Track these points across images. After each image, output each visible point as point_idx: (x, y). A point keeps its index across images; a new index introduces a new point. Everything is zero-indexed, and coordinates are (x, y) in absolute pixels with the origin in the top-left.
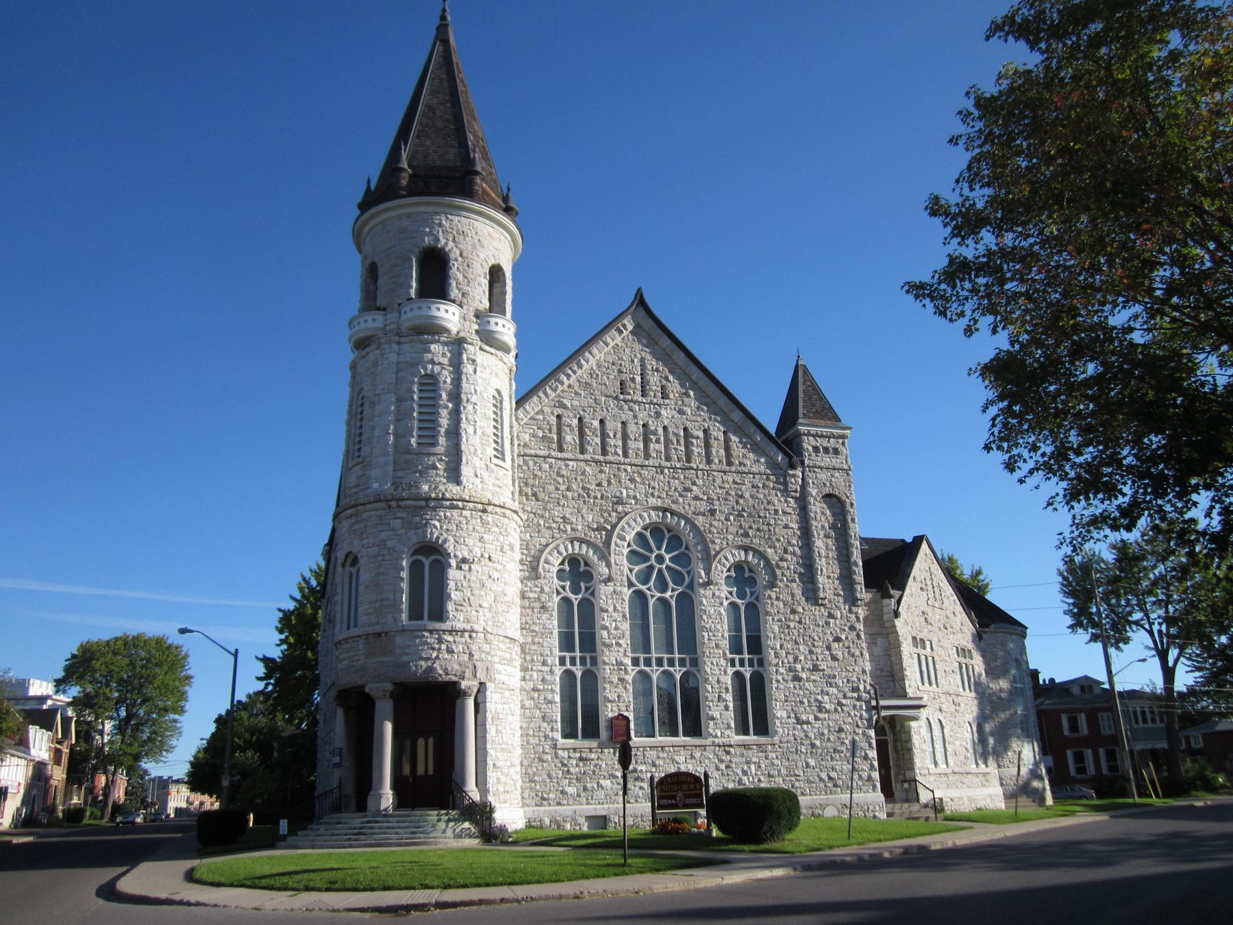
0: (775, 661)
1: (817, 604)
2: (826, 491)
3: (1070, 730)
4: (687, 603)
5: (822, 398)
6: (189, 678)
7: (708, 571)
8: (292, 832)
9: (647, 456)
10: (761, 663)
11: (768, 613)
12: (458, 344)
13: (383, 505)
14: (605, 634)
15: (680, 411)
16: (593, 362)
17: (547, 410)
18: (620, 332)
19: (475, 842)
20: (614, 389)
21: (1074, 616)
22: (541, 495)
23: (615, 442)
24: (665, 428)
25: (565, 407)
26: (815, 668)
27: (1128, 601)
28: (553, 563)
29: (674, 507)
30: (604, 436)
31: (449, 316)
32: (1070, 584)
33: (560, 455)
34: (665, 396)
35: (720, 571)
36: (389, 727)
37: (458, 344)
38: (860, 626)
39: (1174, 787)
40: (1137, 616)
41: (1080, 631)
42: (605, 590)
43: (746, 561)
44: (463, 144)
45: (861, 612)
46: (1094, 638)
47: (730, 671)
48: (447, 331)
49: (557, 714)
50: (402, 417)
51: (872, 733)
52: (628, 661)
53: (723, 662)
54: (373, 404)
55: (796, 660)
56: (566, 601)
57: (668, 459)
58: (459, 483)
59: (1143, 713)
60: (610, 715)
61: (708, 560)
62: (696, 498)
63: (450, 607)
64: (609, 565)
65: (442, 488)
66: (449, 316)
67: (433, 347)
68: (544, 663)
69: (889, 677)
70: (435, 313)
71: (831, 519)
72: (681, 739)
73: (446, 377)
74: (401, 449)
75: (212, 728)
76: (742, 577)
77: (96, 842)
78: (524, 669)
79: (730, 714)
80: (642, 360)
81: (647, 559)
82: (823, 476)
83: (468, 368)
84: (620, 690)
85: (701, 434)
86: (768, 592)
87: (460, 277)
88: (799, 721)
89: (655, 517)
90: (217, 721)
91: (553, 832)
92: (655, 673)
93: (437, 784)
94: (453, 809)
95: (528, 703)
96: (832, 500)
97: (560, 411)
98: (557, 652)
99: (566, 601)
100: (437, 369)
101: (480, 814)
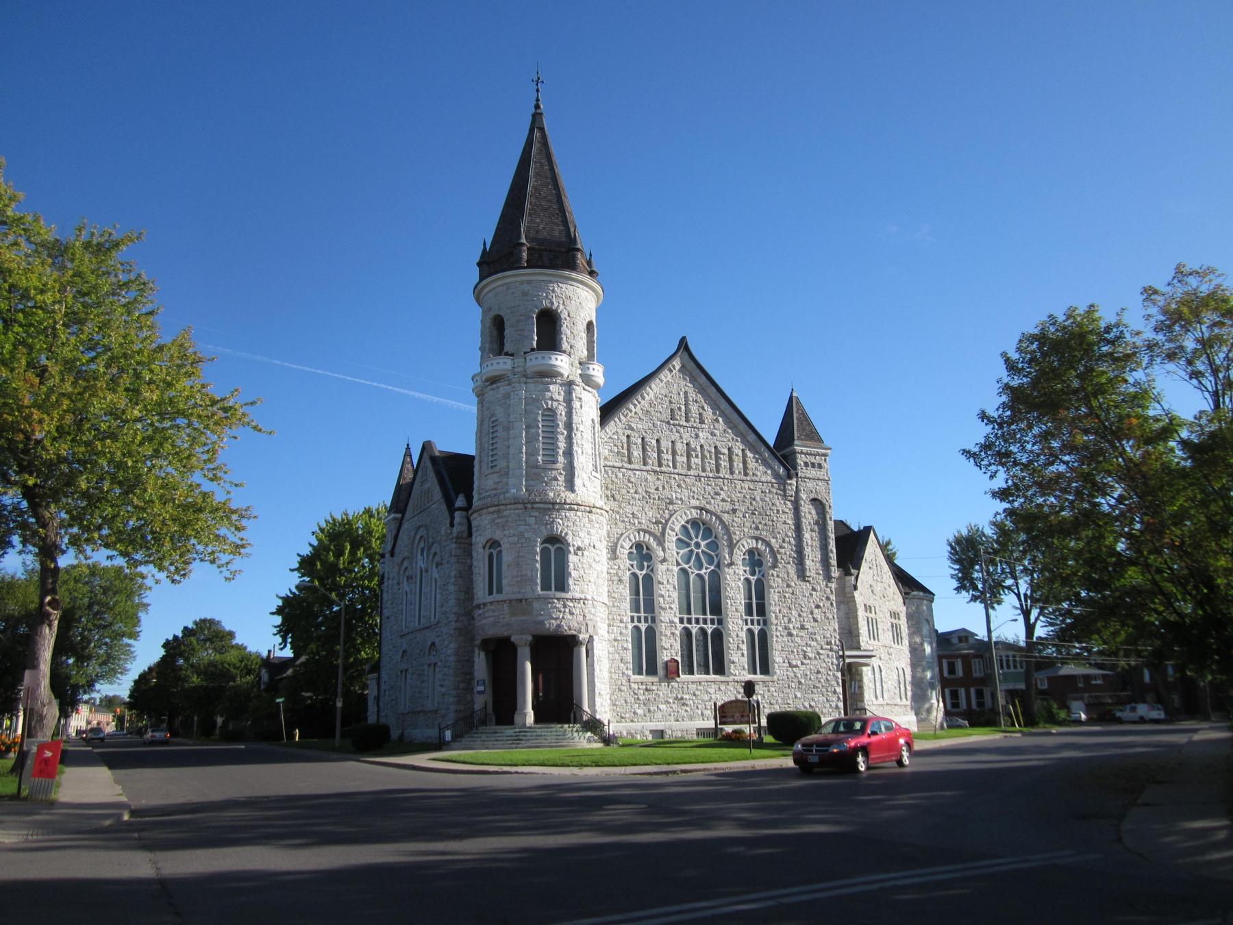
0: (775, 622)
1: (804, 580)
2: (813, 496)
3: (960, 672)
4: (716, 579)
5: (810, 424)
6: (146, 605)
7: (731, 554)
8: (456, 737)
9: (689, 468)
10: (765, 623)
11: (771, 587)
12: (569, 385)
13: (521, 506)
14: (661, 600)
15: (713, 434)
16: (652, 394)
17: (620, 431)
18: (671, 371)
19: (600, 745)
20: (666, 415)
21: (959, 579)
22: (617, 497)
23: (667, 457)
24: (702, 446)
25: (632, 429)
26: (803, 627)
27: (1003, 569)
28: (625, 547)
29: (708, 507)
30: (660, 452)
31: (562, 363)
32: (956, 553)
33: (630, 466)
34: (702, 422)
35: (739, 556)
36: (528, 666)
37: (569, 385)
38: (833, 597)
39: (1030, 721)
40: (1009, 582)
41: (964, 593)
42: (661, 568)
43: (757, 548)
44: (565, 222)
45: (833, 586)
46: (974, 599)
47: (745, 628)
48: (562, 375)
49: (629, 656)
50: (531, 440)
51: (839, 675)
52: (677, 620)
53: (740, 622)
54: (507, 429)
55: (790, 621)
56: (634, 575)
57: (704, 470)
58: (573, 491)
59: (1008, 661)
60: (666, 659)
61: (732, 546)
62: (723, 500)
63: (571, 581)
64: (664, 550)
65: (563, 495)
66: (562, 363)
67: (551, 387)
68: (621, 621)
69: (849, 635)
70: (553, 362)
71: (816, 517)
72: (712, 677)
73: (562, 410)
74: (533, 465)
75: (162, 652)
76: (755, 561)
77: (129, 753)
78: (609, 625)
79: (745, 659)
80: (686, 393)
81: (688, 545)
82: (810, 484)
83: (576, 404)
84: (672, 641)
85: (726, 451)
86: (771, 572)
87: (568, 332)
88: (791, 665)
89: (695, 514)
90: (165, 646)
91: (629, 740)
92: (694, 629)
93: (561, 704)
94: (575, 722)
95: (612, 650)
96: (818, 503)
97: (628, 432)
98: (629, 614)
99: (634, 575)
100: (555, 404)
101: (594, 725)
